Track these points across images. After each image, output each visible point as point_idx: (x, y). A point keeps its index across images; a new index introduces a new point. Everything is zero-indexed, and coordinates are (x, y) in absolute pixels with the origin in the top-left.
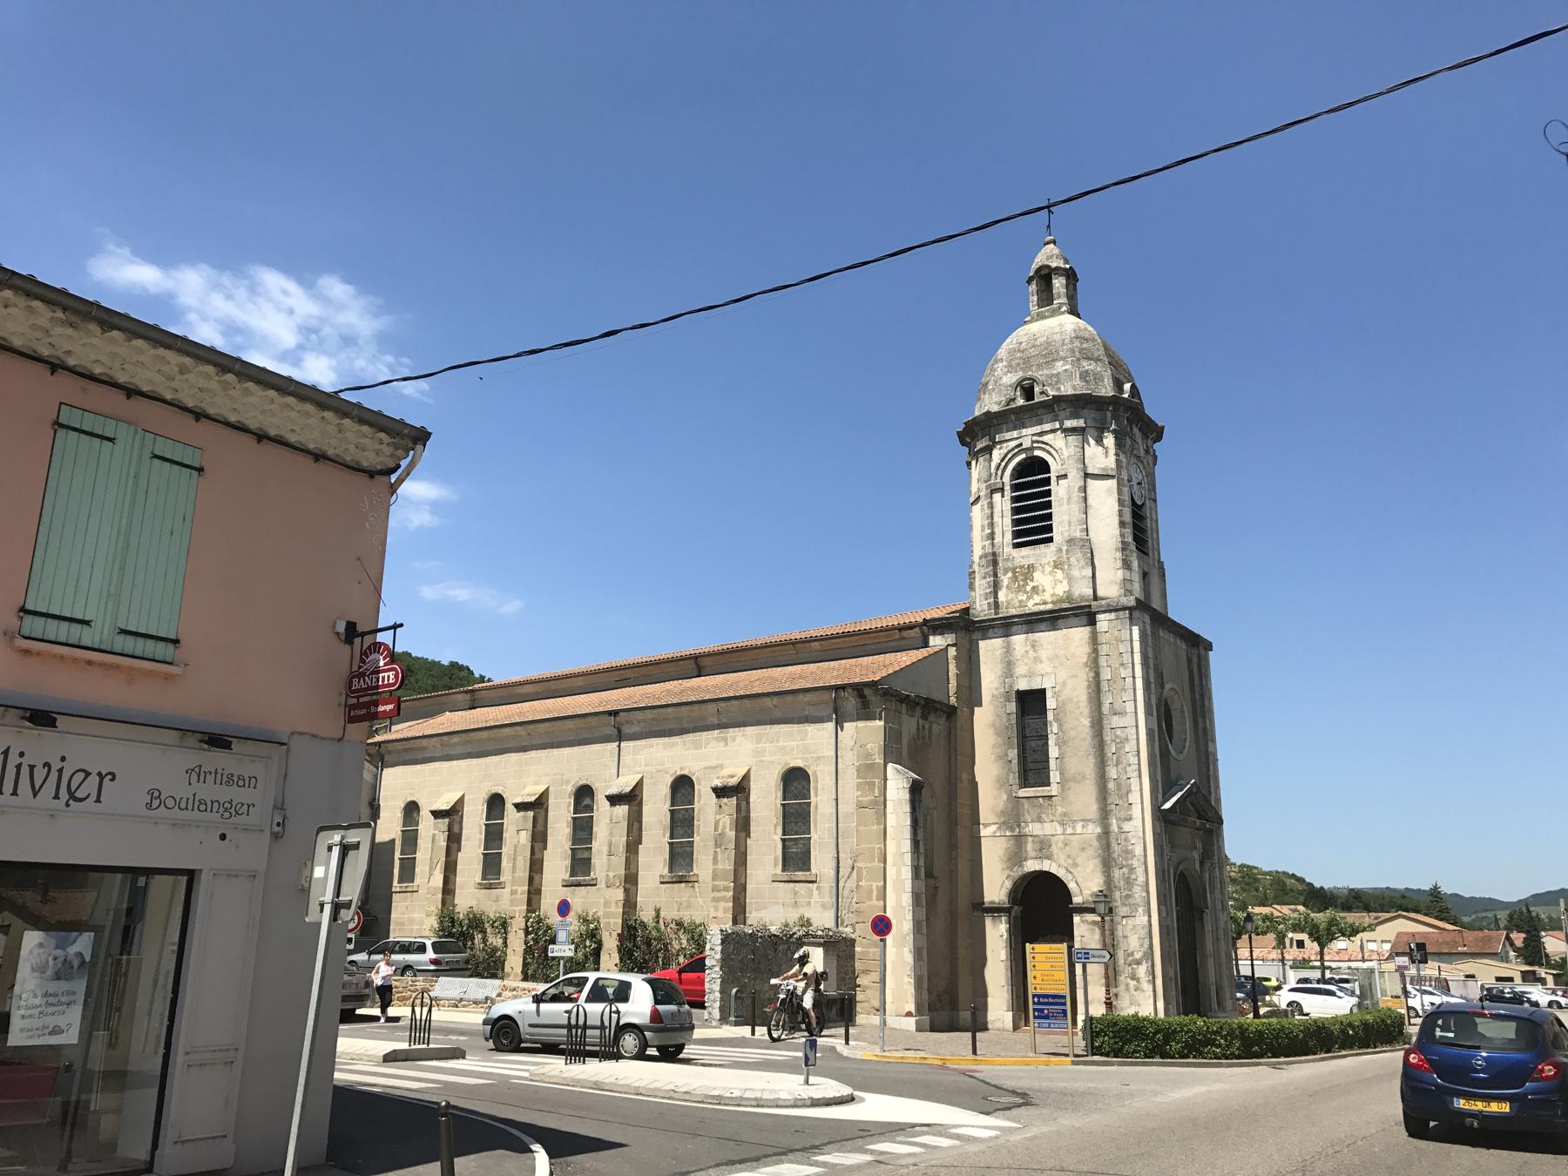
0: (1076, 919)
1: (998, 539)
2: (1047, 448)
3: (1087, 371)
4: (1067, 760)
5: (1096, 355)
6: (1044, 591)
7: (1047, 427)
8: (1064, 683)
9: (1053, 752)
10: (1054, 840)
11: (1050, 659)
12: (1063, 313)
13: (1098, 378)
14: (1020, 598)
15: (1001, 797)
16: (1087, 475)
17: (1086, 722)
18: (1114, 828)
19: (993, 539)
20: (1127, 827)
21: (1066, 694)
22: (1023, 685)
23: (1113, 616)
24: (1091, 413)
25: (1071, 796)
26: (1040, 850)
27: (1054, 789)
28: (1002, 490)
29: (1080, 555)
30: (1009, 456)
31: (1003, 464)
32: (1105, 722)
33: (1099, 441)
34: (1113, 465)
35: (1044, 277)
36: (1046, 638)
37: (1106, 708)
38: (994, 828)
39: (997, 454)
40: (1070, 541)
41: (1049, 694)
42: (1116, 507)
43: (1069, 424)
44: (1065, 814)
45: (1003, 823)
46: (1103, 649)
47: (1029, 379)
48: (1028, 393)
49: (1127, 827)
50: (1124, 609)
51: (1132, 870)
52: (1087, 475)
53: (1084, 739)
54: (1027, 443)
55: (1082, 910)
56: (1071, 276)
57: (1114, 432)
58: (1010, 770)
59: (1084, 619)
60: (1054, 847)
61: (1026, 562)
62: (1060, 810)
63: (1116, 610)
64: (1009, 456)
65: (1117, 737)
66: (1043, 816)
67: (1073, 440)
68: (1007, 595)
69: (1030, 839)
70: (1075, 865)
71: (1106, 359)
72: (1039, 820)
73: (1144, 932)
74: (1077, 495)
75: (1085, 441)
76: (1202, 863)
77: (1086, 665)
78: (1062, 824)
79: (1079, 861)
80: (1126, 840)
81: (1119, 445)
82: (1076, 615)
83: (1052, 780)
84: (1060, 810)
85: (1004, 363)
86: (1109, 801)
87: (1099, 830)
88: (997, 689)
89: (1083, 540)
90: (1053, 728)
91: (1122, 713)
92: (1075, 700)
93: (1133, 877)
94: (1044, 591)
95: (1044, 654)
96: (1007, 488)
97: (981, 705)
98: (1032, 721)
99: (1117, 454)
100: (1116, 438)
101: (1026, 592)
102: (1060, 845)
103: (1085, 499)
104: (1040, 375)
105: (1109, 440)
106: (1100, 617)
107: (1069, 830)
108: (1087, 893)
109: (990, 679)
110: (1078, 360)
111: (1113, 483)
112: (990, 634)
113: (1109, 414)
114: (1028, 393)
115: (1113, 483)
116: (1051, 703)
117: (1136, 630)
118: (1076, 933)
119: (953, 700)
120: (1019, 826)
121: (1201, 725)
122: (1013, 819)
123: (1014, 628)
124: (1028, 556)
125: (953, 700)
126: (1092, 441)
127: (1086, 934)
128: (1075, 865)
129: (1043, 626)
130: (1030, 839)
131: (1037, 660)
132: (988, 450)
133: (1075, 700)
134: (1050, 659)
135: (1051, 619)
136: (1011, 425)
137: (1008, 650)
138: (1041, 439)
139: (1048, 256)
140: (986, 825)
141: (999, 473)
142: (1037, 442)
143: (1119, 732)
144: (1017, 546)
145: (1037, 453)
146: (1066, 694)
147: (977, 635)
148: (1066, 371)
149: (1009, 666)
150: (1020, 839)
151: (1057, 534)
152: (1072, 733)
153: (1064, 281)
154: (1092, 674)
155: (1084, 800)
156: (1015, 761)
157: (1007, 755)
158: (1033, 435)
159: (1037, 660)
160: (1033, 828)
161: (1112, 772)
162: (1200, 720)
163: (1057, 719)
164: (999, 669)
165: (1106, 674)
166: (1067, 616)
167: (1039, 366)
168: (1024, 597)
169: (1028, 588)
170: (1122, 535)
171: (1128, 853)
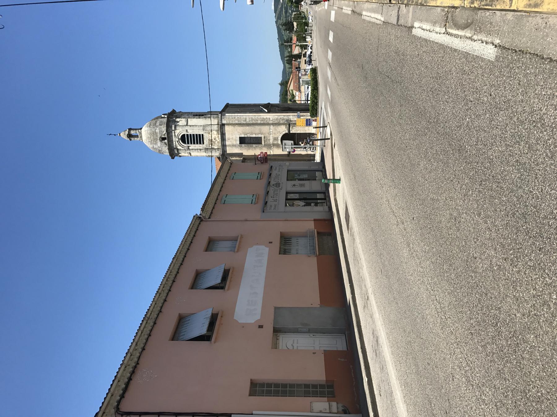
0: (291, 132)
1: (201, 148)
2: (179, 134)
3: (159, 124)
4: (256, 133)
5: (155, 122)
6: (215, 137)
7: (173, 134)
8: (238, 132)
9: (254, 136)
10: (274, 137)
11: (232, 135)
12: (141, 131)
13: (161, 122)
14: (217, 143)
15: (264, 149)
16: (187, 125)
17: (247, 127)
18: (271, 122)
19: (201, 149)
20: (271, 119)
21: (241, 132)
22: (238, 142)
23: (223, 119)
24: (171, 124)
25: (264, 132)
26: (276, 140)
27: (263, 136)
28: (189, 146)
29: (207, 128)
30: (180, 144)
31: (182, 146)
32: (248, 123)
33: (178, 122)
34: (184, 119)
35: (130, 136)
36: (227, 136)
37: (245, 122)
38: (271, 151)
39: (179, 147)
40: (203, 130)
41: (241, 136)
42: (195, 119)
43: (173, 128)
44: (268, 134)
45: (270, 148)
46: (231, 122)
47: (160, 138)
48: (163, 139)
49: (271, 119)
50: (221, 117)
51: (281, 119)
52: (187, 125)
53: (251, 128)
54: (177, 140)
55: (289, 131)
56: (130, 129)
57: (176, 118)
58: (258, 147)
59: (223, 127)
60: (276, 137)
61: (208, 141)
62: (267, 135)
63: (222, 119)
64: (180, 144)
65: (251, 120)
66: (269, 139)
67: (177, 128)
68: (216, 146)
69: (274, 142)
70: (279, 132)
71: (156, 120)
72: (269, 140)
73: (294, 117)
74: (192, 128)
75: (178, 125)
76: (279, 107)
77: (234, 127)
78: (270, 134)
79: (278, 131)
80: (274, 119)
81: (179, 118)
82: (222, 129)
83: (260, 136)
84: (267, 135)
85: (154, 145)
86: (266, 123)
87: (272, 126)
88: (239, 149)
89: (203, 127)
90: (249, 135)
91: (246, 119)
92: (242, 130)
93: (282, 118)
94: (215, 137)
95: (231, 137)
96: (188, 145)
97: (242, 153)
98: (247, 141)
99: (182, 118)
100: (178, 118)
101: (215, 141)
102: (275, 135)
103: (193, 126)
104: (159, 136)
105: (178, 120)
106: (223, 123)
107: (272, 133)
108: (286, 129)
109: (236, 150)
110: (156, 126)
111: (189, 120)
112: (226, 150)
113: (171, 119)
114: (163, 139)
115: (189, 120)
116: (243, 136)
117: (226, 114)
118: (294, 132)
119: (242, 159)
120: (271, 145)
121: (247, 106)
122: (269, 146)
123: (224, 144)
124: (206, 140)
125: (242, 159)
126: (178, 124)
127: (294, 130)
128: (279, 132)
129: (224, 137)
130: (274, 142)
131: (232, 139)
132: (178, 150)
133: (242, 130)
134: (232, 135)
135: (223, 135)
136: (172, 144)
137: (229, 146)
138: (176, 136)
139: (124, 135)
140: (270, 153)
141: (184, 147)
142: (177, 137)
143: (250, 120)
144: (203, 143)
145: (180, 137)
146: (241, 132)
147: (225, 153)
148: (159, 129)
149: (233, 146)
150: (274, 145)
151: (201, 133)
152: (250, 131)
153: (132, 131)
154: (236, 125)
155: (265, 129)
156: (256, 145)
157: (255, 147)
158: (175, 138)
159: (232, 139)
160: (271, 141)
161: (259, 122)
162: (246, 106)
163: (246, 135)
164: (234, 148)
165: (237, 122)
166: (224, 149)
167: (157, 136)
168: (216, 142)
169: (214, 141)
170: (202, 118)
171: (277, 119)
